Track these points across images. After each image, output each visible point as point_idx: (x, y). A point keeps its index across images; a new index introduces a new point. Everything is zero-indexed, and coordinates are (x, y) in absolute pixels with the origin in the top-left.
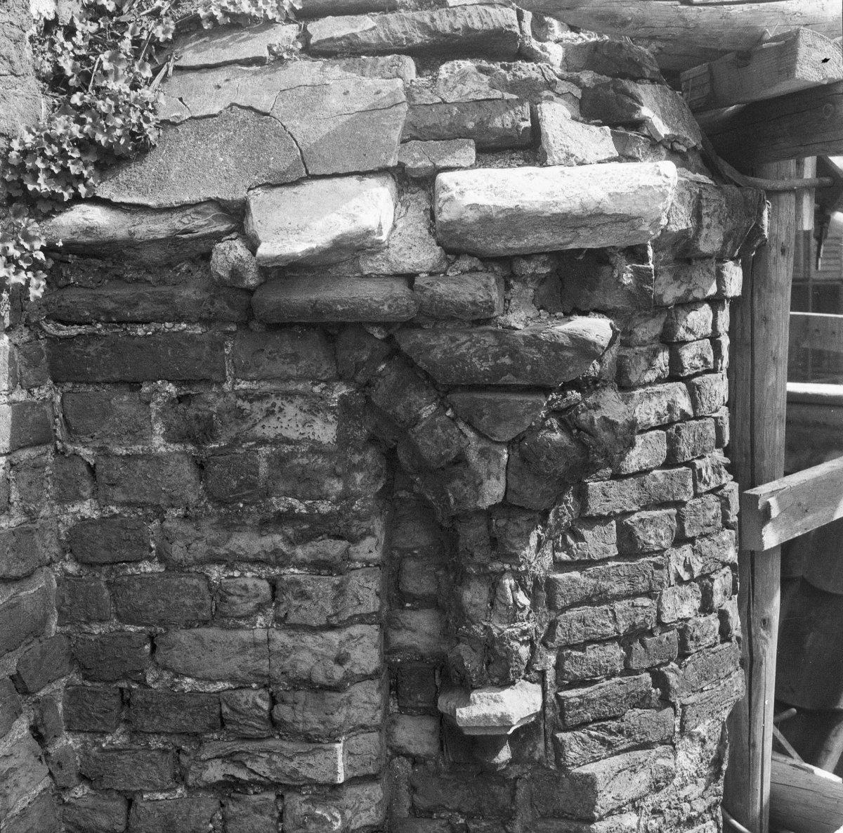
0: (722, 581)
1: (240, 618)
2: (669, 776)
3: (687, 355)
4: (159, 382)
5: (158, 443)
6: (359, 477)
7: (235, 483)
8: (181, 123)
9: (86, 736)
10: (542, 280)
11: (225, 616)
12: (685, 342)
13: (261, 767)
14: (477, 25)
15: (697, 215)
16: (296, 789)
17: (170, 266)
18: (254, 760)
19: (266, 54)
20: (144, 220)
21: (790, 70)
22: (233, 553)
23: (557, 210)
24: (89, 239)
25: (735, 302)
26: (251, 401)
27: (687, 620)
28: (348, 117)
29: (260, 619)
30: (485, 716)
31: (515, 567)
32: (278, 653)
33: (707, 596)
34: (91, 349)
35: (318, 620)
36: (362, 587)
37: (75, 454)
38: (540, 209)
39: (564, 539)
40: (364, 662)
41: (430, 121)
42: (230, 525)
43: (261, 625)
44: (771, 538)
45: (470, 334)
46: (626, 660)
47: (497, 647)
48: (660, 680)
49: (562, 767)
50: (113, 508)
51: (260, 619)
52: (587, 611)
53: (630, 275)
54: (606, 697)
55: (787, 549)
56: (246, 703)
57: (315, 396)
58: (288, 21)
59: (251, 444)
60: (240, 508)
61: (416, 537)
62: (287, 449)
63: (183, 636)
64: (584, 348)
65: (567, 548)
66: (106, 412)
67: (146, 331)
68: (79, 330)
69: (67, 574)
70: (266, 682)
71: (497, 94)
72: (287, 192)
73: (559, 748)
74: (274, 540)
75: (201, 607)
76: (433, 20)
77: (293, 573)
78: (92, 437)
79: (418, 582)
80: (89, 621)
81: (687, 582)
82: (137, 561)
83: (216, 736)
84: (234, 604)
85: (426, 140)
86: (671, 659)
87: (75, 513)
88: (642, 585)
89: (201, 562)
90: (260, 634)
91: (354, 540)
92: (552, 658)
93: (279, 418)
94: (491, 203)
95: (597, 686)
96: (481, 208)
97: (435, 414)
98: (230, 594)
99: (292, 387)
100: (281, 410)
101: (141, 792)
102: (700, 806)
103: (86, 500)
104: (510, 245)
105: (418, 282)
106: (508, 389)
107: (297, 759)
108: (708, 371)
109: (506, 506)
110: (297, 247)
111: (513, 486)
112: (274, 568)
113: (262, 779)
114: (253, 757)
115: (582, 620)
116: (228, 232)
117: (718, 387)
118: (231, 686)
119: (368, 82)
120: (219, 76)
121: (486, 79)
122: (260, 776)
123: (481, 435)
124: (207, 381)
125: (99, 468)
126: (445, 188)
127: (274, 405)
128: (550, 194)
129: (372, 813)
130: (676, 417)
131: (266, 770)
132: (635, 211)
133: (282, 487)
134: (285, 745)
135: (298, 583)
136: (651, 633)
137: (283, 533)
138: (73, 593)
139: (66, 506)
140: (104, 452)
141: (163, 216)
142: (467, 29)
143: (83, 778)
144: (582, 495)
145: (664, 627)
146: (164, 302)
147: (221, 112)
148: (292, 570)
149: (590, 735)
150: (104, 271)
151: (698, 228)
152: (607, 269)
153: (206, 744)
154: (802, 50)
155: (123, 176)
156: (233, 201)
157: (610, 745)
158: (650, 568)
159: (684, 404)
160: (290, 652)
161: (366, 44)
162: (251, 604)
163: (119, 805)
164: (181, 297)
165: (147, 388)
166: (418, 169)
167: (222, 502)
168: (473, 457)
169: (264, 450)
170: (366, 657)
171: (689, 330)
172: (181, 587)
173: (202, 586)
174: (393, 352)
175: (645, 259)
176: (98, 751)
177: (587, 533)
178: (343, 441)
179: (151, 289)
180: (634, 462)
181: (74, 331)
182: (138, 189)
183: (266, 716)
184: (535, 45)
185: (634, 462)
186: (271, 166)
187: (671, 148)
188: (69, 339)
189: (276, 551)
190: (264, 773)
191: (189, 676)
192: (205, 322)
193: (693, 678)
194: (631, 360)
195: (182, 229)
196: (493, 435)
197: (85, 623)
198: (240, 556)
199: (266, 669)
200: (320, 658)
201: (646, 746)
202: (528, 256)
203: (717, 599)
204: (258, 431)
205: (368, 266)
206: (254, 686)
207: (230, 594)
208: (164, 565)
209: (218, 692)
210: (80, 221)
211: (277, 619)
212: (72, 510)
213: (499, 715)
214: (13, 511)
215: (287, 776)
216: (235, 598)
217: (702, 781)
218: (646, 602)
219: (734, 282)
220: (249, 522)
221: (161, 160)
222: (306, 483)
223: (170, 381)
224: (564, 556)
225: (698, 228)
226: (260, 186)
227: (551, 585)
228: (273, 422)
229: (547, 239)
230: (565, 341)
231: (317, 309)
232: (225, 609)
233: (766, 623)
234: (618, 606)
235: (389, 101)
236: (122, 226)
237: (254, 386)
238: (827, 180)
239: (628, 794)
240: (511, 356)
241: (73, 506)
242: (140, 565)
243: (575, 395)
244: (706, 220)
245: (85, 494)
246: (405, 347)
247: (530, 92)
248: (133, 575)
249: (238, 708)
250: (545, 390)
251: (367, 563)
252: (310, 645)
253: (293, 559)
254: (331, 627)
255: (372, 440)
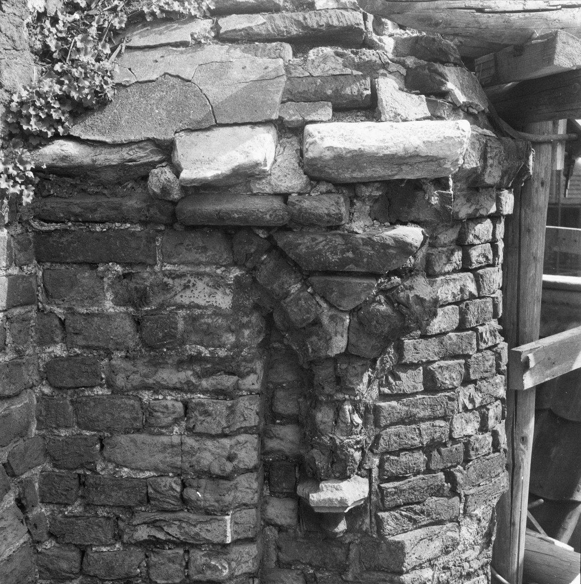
0: (494, 410)
1: (162, 427)
2: (455, 544)
3: (475, 254)
4: (110, 264)
5: (109, 306)
6: (247, 332)
7: (161, 335)
8: (130, 86)
9: (54, 507)
10: (376, 200)
11: (152, 426)
12: (473, 245)
13: (174, 531)
14: (335, 23)
15: (484, 157)
16: (197, 547)
17: (120, 184)
18: (169, 525)
19: (189, 39)
20: (103, 152)
21: (550, 60)
22: (158, 383)
23: (387, 152)
24: (64, 164)
25: (508, 218)
26: (173, 279)
27: (470, 436)
28: (245, 84)
29: (176, 429)
30: (330, 500)
31: (352, 397)
32: (188, 453)
33: (484, 419)
34: (63, 240)
35: (215, 430)
36: (247, 408)
37: (51, 312)
38: (376, 151)
39: (387, 379)
40: (246, 460)
41: (301, 89)
42: (156, 364)
43: (176, 433)
44: (529, 381)
45: (326, 236)
46: (428, 463)
47: (339, 452)
48: (450, 477)
49: (382, 536)
50: (76, 350)
51: (176, 429)
52: (401, 429)
53: (436, 198)
54: (413, 488)
55: (540, 389)
56: (165, 486)
57: (217, 276)
58: (205, 17)
59: (172, 308)
60: (164, 352)
61: (286, 375)
62: (197, 312)
63: (123, 439)
64: (404, 248)
65: (388, 385)
66: (73, 283)
67: (102, 229)
68: (56, 226)
69: (44, 394)
70: (179, 472)
71: (348, 71)
72: (202, 135)
73: (380, 522)
74: (186, 375)
75: (135, 419)
76: (305, 19)
77: (199, 398)
78: (63, 301)
79: (286, 405)
80: (58, 427)
81: (471, 411)
82: (92, 387)
83: (143, 509)
84: (158, 417)
85: (298, 102)
86: (458, 463)
87: (50, 353)
88: (440, 412)
89: (136, 389)
90: (176, 440)
91: (242, 376)
92: (377, 461)
93: (192, 291)
94: (342, 146)
95: (407, 480)
96: (335, 150)
97: (300, 291)
98: (156, 411)
99: (202, 269)
100: (194, 285)
101: (91, 546)
102: (476, 565)
103: (58, 343)
104: (355, 175)
105: (290, 199)
106: (350, 274)
107: (199, 526)
108: (489, 266)
109: (347, 355)
110: (208, 173)
111: (353, 341)
112: (186, 394)
113: (175, 539)
114: (169, 524)
115: (398, 435)
116: (160, 162)
117: (495, 277)
118: (155, 474)
119: (260, 60)
120: (156, 54)
121: (340, 60)
122: (173, 537)
123: (331, 306)
124: (143, 264)
125: (67, 322)
126: (310, 135)
127: (189, 281)
128: (383, 141)
129: (250, 564)
130: (466, 297)
131: (178, 533)
132: (441, 154)
133: (193, 338)
134: (191, 516)
135: (203, 405)
136: (445, 445)
137: (193, 370)
138: (48, 408)
139: (44, 347)
140: (71, 311)
141: (116, 150)
142: (329, 26)
143: (51, 535)
144: (400, 349)
145: (454, 441)
146: (115, 209)
147: (157, 79)
148: (199, 395)
149: (401, 514)
150: (74, 186)
151: (484, 167)
152: (420, 194)
153: (136, 514)
154: (559, 46)
155: (89, 121)
156: (164, 140)
157: (415, 521)
158: (446, 400)
159: (472, 287)
160: (196, 452)
161: (258, 34)
162: (170, 418)
163: (75, 555)
164: (127, 205)
165: (102, 268)
166: (293, 121)
167: (151, 348)
168: (325, 320)
169: (182, 313)
170: (248, 456)
171: (477, 237)
172: (122, 406)
173: (137, 405)
174: (273, 247)
175: (447, 187)
176: (62, 517)
177: (402, 375)
178: (236, 307)
179: (106, 200)
180: (436, 327)
181: (52, 227)
182: (99, 131)
183: (178, 495)
184: (375, 38)
185: (436, 327)
186: (191, 117)
187: (467, 112)
188: (49, 233)
189: (188, 382)
190: (176, 535)
191: (126, 467)
192: (144, 223)
193: (473, 476)
194: (436, 257)
195: (128, 158)
196: (340, 306)
197: (56, 428)
198: (162, 385)
199: (179, 463)
200: (217, 457)
201: (440, 522)
202: (367, 183)
203: (491, 423)
204: (178, 299)
205: (257, 187)
206: (171, 474)
207: (156, 411)
208: (110, 390)
209: (146, 479)
210: (58, 152)
211: (188, 429)
212: (48, 350)
213: (339, 499)
214: (8, 350)
215: (192, 537)
216: (159, 414)
217: (478, 548)
218: (442, 423)
219: (508, 202)
220: (170, 361)
221: (115, 111)
222: (209, 335)
223: (117, 263)
224: (386, 390)
225: (484, 167)
226: (183, 130)
227: (377, 410)
228: (188, 293)
229: (380, 172)
230: (390, 242)
231: (221, 216)
232: (152, 421)
233: (524, 440)
234: (423, 426)
235: (274, 74)
236: (88, 156)
237: (176, 268)
238: (574, 136)
239: (427, 556)
240: (354, 253)
241: (49, 348)
242: (94, 389)
243: (396, 280)
244: (490, 161)
245: (57, 339)
246: (280, 244)
247: (371, 70)
248: (89, 396)
249: (159, 490)
250: (376, 276)
251: (251, 392)
252: (210, 447)
253: (200, 388)
254: (224, 435)
255: (256, 307)
